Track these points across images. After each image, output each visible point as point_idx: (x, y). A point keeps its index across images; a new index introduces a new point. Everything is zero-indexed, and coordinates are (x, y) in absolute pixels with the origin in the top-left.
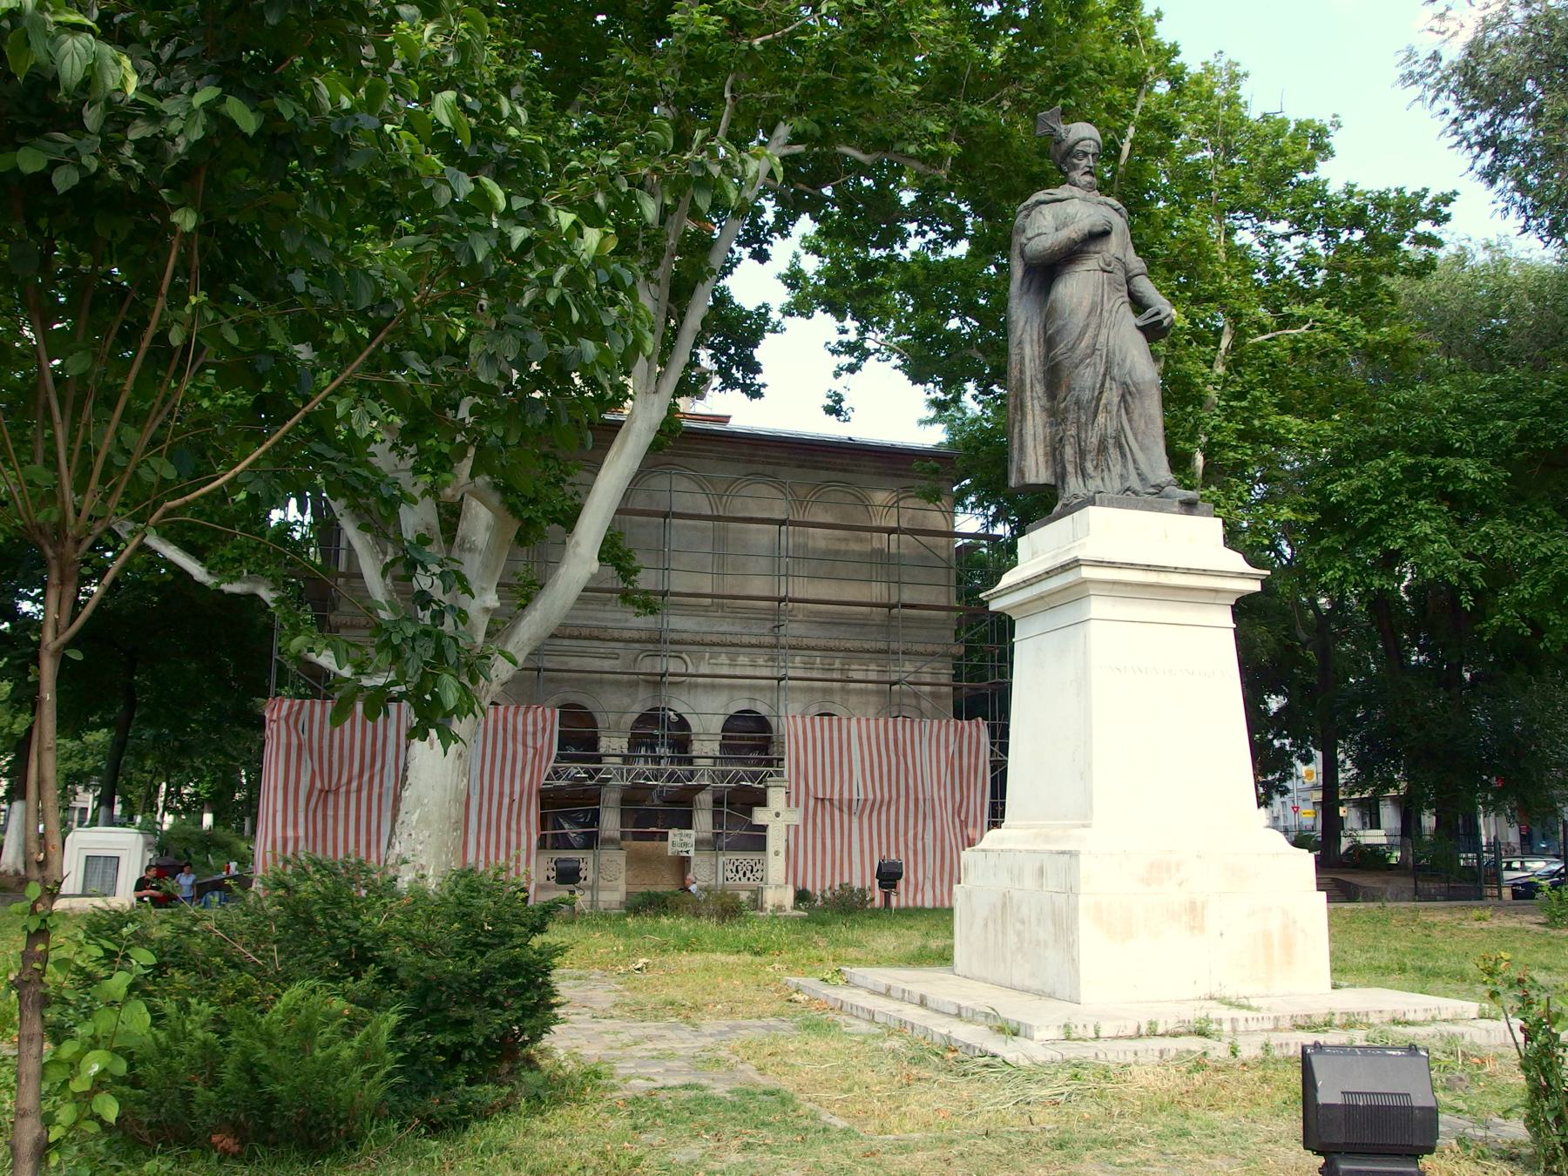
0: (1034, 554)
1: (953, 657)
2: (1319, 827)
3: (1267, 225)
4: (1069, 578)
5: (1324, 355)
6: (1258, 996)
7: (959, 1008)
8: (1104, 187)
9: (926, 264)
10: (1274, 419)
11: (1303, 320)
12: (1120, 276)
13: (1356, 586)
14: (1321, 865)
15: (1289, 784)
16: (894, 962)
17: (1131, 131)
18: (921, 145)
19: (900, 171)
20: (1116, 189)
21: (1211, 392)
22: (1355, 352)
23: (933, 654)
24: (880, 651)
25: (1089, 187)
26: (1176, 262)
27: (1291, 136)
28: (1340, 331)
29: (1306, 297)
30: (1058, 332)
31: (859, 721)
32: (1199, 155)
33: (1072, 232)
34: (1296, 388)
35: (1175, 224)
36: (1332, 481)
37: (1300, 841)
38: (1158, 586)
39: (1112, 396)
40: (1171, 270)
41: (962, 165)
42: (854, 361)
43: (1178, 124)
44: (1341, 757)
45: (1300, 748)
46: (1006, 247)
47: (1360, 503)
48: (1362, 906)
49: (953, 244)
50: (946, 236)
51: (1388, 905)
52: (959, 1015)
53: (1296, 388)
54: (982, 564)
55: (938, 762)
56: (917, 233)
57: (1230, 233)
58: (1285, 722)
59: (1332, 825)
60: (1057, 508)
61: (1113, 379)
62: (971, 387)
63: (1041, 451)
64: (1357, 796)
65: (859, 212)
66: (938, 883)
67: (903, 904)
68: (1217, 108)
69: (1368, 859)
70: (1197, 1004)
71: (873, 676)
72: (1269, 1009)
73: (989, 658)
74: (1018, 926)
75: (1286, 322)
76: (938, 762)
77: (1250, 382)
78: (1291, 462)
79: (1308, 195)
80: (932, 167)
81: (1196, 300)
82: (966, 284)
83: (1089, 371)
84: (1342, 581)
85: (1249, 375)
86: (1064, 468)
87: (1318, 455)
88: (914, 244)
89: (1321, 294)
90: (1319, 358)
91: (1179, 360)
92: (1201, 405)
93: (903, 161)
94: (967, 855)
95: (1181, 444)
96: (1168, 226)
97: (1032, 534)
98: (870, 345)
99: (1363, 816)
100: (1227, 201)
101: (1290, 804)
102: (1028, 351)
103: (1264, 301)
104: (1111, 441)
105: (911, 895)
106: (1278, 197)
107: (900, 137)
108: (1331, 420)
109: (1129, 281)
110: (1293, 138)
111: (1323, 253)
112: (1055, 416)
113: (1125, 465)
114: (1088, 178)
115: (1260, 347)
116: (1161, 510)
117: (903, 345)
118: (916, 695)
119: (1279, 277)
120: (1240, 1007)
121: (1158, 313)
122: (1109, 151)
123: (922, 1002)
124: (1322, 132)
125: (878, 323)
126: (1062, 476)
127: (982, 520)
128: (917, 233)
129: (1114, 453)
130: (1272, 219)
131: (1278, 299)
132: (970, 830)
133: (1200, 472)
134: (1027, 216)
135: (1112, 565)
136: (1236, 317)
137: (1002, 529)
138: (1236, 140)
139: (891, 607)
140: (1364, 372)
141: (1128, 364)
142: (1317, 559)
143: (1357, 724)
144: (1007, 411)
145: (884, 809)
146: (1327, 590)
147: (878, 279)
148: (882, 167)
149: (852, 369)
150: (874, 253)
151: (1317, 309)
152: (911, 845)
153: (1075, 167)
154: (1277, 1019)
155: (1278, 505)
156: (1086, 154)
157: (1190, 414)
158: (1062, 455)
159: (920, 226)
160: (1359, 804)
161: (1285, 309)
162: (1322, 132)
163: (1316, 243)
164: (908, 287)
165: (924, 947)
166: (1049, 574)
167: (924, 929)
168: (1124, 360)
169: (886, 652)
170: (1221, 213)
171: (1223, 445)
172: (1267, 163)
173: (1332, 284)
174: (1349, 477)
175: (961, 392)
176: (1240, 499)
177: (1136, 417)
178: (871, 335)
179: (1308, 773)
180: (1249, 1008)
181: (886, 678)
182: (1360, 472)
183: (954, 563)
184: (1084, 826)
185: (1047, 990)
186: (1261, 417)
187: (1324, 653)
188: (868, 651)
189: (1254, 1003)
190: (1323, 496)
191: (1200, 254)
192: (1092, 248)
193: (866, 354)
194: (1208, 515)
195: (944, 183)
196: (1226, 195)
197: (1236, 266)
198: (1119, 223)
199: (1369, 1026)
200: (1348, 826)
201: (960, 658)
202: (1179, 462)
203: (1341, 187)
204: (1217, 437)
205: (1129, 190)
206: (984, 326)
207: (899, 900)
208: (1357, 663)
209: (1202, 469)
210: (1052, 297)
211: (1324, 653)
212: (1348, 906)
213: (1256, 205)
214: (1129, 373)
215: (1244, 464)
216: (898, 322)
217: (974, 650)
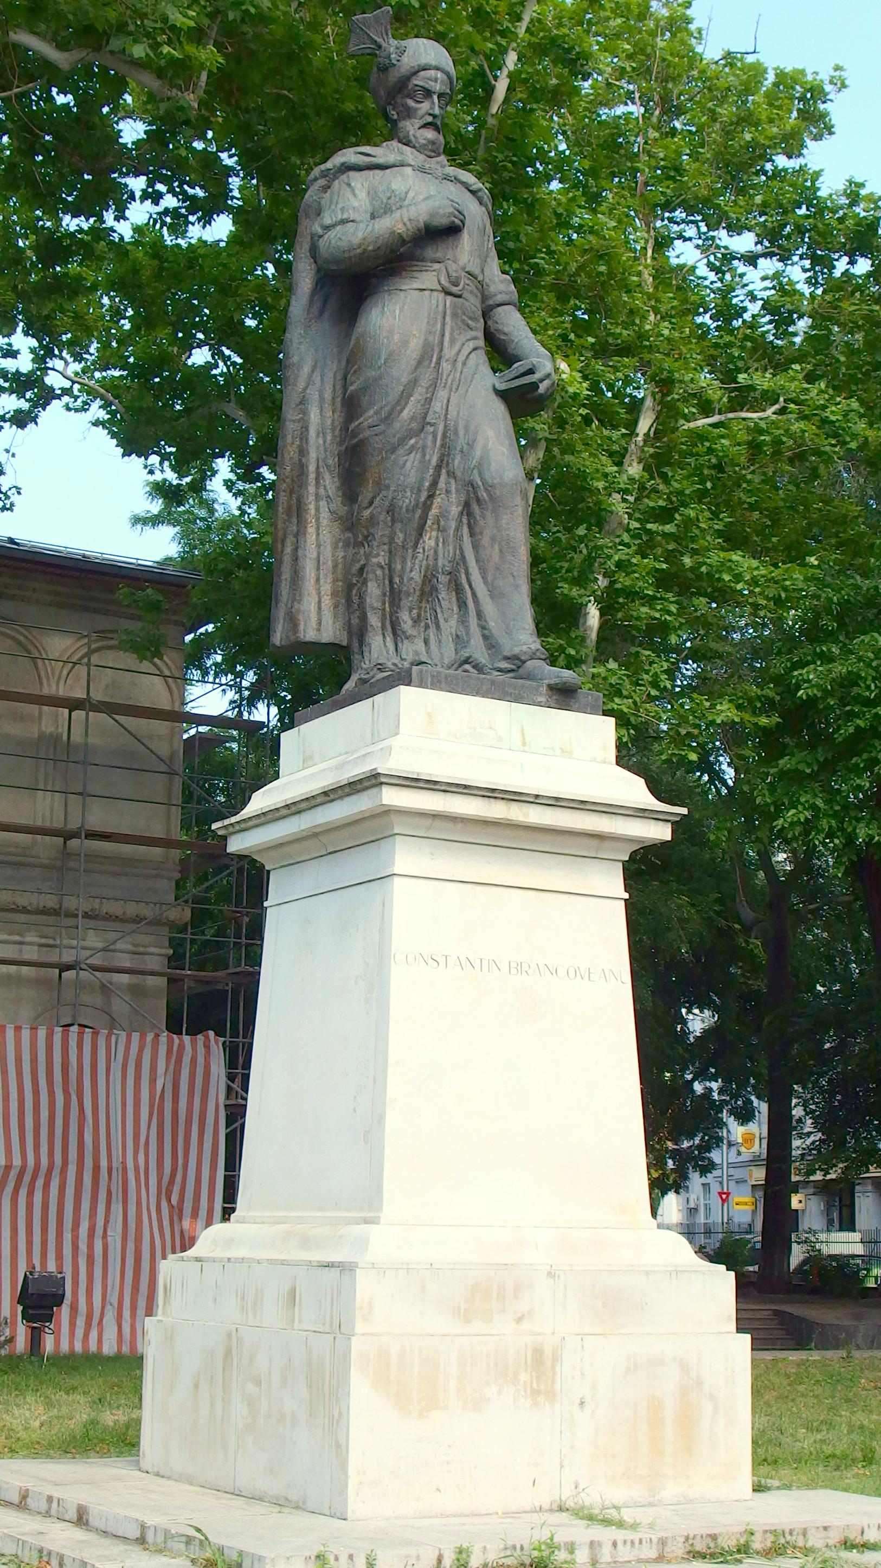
0: (307, 761)
1: (171, 925)
2: (759, 1227)
3: (723, 237)
4: (360, 804)
5: (798, 457)
6: (637, 1505)
7: (143, 1527)
8: (457, 151)
9: (158, 250)
10: (715, 557)
11: (770, 398)
12: (473, 304)
13: (831, 835)
14: (743, 1288)
15: (715, 1156)
16: (40, 1449)
17: (511, 59)
18: (156, 46)
19: (120, 85)
20: (481, 153)
21: (618, 505)
22: (850, 456)
23: (138, 920)
24: (45, 912)
25: (431, 150)
26: (572, 285)
27: (767, 95)
28: (825, 421)
29: (776, 360)
30: (365, 389)
31: (18, 1029)
32: (620, 110)
34: (752, 508)
35: (576, 221)
36: (802, 664)
37: (722, 1250)
38: (505, 826)
39: (448, 503)
40: (562, 297)
41: (225, 86)
42: (24, 405)
43: (586, 56)
44: (798, 1112)
45: (734, 1096)
46: (290, 234)
47: (843, 702)
48: (815, 1356)
49: (206, 220)
50: (194, 205)
51: (856, 1354)
52: (141, 1541)
53: (752, 508)
54: (228, 769)
55: (137, 1104)
56: (145, 196)
57: (662, 243)
58: (714, 1052)
59: (778, 1220)
60: (349, 685)
62: (224, 467)
63: (326, 588)
64: (818, 1176)
65: (46, 150)
66: (127, 1313)
67: (65, 1347)
68: (653, 34)
69: (832, 1279)
70: (536, 1518)
71: (31, 954)
72: (651, 1526)
73: (231, 931)
74: (250, 1387)
75: (743, 398)
76: (137, 1104)
77: (680, 493)
78: (743, 628)
79: (789, 193)
80: (172, 86)
81: (602, 351)
82: (225, 291)
83: (412, 461)
84: (808, 826)
85: (680, 481)
86: (364, 618)
87: (781, 619)
88: (139, 212)
89: (800, 357)
90: (791, 461)
91: (569, 449)
92: (600, 524)
93: (124, 69)
94: (169, 1267)
95: (565, 588)
96: (563, 223)
97: (304, 727)
98: (54, 380)
99: (828, 1211)
100: (665, 189)
101: (715, 1188)
102: (314, 417)
103: (710, 361)
104: (443, 579)
105: (79, 1333)
106: (741, 192)
107: (121, 28)
108: (804, 565)
109: (487, 313)
110: (771, 98)
111: (806, 290)
112: (354, 530)
113: (463, 621)
114: (430, 134)
115: (699, 436)
116: (518, 699)
117: (111, 386)
118: (105, 989)
119: (737, 323)
120: (606, 1522)
121: (531, 371)
122: (475, 89)
123: (82, 1519)
124: (816, 93)
125: (71, 344)
126: (359, 633)
127: (231, 695)
128: (145, 196)
129: (446, 596)
130: (729, 228)
131: (732, 359)
132: (186, 1224)
133: (594, 636)
134: (326, 188)
135: (432, 785)
136: (664, 384)
137: (264, 713)
138: (680, 91)
139: (68, 836)
140: (862, 489)
141: (478, 452)
142: (772, 788)
143: (823, 1058)
144: (280, 509)
145: (23, 1192)
146: (787, 842)
147: (73, 267)
148: (89, 75)
149: (21, 420)
150: (71, 223)
151: (792, 381)
152: (83, 1246)
153: (409, 113)
154: (663, 1542)
155: (714, 697)
156: (428, 93)
157: (581, 539)
158: (361, 597)
159: (151, 183)
160: (824, 1189)
161: (742, 377)
162: (816, 93)
163: (797, 273)
164: (126, 286)
165: (93, 1422)
166: (330, 795)
167: (95, 1392)
168: (471, 445)
169: (55, 912)
170: (652, 209)
171: (632, 594)
172: (728, 134)
173: (818, 342)
174: (828, 659)
175: (207, 472)
176: (655, 684)
177: (486, 541)
178: (58, 364)
179: (745, 1137)
180: (620, 1524)
181: (54, 959)
182: (846, 651)
183: (179, 766)
184: (367, 1221)
185: (294, 1496)
186: (694, 552)
187: (779, 945)
188: (24, 910)
189: (627, 1515)
190: (787, 686)
191: (611, 275)
192: (429, 253)
193: (46, 396)
194: (593, 712)
195: (193, 114)
196: (659, 181)
197: (669, 301)
198: (476, 214)
199: (807, 1551)
200: (804, 1224)
201: (183, 929)
202: (554, 616)
203: (840, 186)
204: (623, 581)
205: (500, 160)
206: (251, 364)
207: (61, 1337)
208: (830, 960)
209: (579, 638)
210: (359, 329)
211: (779, 945)
212: (794, 1356)
213: (707, 201)
214: (479, 467)
215: (663, 628)
216: (105, 346)
217: (210, 915)
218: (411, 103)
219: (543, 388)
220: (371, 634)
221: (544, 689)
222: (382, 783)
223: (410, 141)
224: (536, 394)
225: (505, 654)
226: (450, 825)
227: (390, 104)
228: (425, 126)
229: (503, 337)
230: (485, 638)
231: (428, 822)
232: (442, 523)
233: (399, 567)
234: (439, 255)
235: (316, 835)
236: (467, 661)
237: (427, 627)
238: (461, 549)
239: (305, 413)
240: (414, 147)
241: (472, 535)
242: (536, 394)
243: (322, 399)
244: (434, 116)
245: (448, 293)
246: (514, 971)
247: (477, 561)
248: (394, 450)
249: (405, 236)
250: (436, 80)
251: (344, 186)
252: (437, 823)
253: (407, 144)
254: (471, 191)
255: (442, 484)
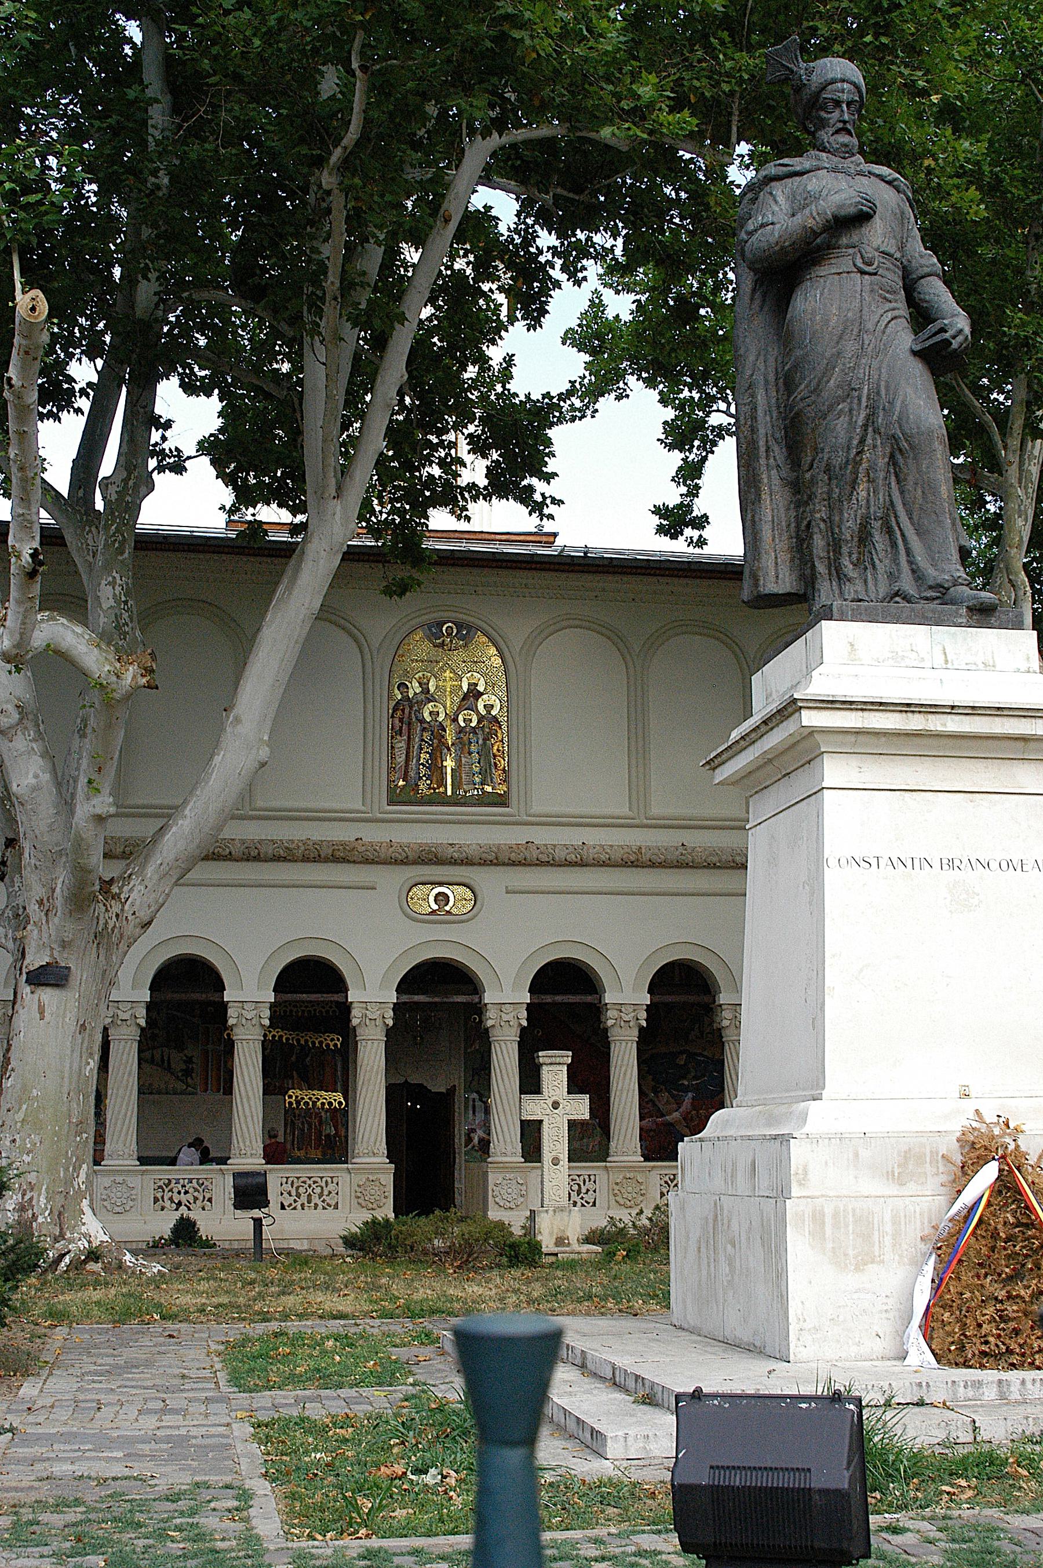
12: (894, 279)
30: (796, 367)
33: (810, 218)
39: (876, 456)
61: (876, 431)
83: (843, 420)
104: (877, 524)
113: (895, 560)
116: (938, 622)
134: (754, 200)
135: (848, 705)
153: (823, 124)
156: (838, 103)
158: (809, 547)
177: (910, 487)
192: (844, 241)
218: (823, 114)
219: (955, 344)
220: (819, 581)
221: (964, 611)
222: (801, 708)
223: (825, 148)
224: (950, 350)
225: (930, 583)
226: (873, 740)
227: (808, 119)
228: (837, 132)
229: (925, 305)
230: (913, 571)
231: (852, 738)
232: (872, 475)
233: (837, 518)
234: (855, 238)
235: (770, 761)
236: (897, 594)
237: (866, 568)
238: (890, 495)
239: (753, 396)
240: (829, 152)
241: (898, 482)
242: (950, 350)
243: (766, 382)
244: (845, 122)
245: (863, 273)
246: (945, 867)
247: (904, 504)
248: (824, 417)
249: (815, 228)
250: (843, 91)
251: (768, 195)
252: (861, 738)
253: (824, 150)
254: (887, 182)
255: (869, 441)
